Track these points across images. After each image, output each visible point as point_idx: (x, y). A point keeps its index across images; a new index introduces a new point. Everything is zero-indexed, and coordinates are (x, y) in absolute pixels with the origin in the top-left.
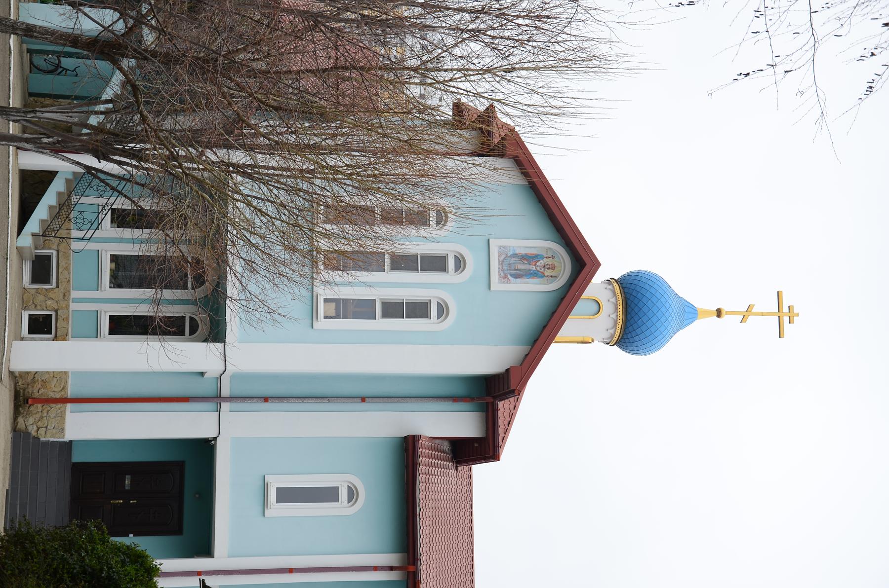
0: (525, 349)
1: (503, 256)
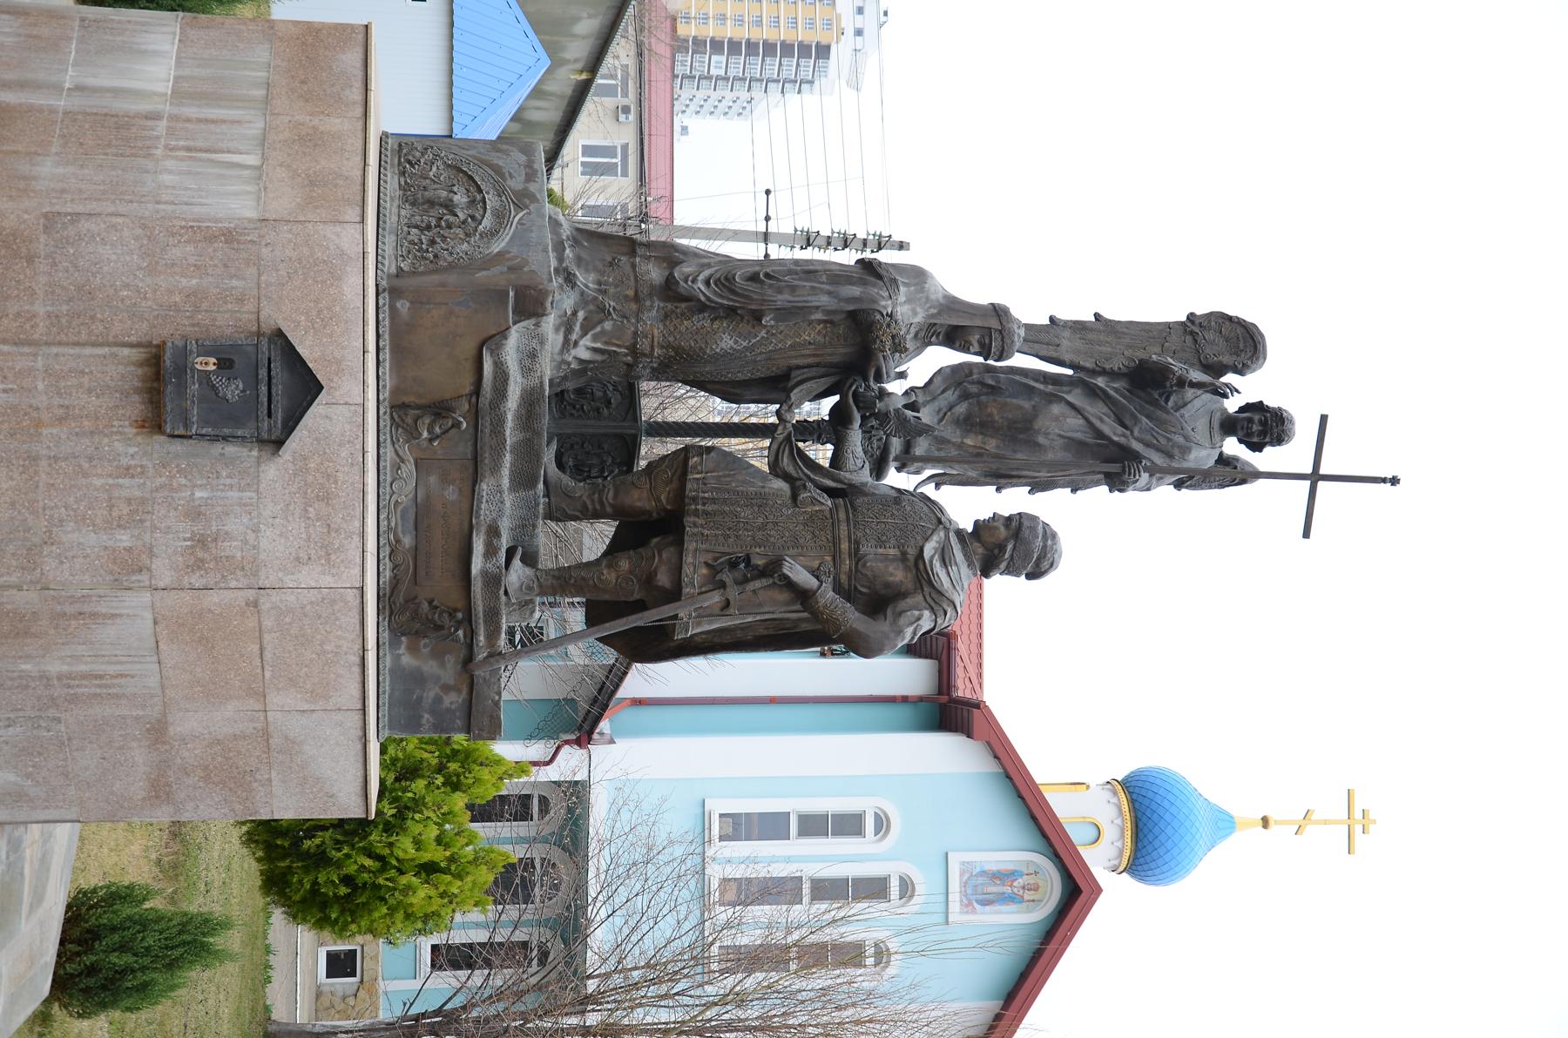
0: (995, 1005)
1: (966, 876)
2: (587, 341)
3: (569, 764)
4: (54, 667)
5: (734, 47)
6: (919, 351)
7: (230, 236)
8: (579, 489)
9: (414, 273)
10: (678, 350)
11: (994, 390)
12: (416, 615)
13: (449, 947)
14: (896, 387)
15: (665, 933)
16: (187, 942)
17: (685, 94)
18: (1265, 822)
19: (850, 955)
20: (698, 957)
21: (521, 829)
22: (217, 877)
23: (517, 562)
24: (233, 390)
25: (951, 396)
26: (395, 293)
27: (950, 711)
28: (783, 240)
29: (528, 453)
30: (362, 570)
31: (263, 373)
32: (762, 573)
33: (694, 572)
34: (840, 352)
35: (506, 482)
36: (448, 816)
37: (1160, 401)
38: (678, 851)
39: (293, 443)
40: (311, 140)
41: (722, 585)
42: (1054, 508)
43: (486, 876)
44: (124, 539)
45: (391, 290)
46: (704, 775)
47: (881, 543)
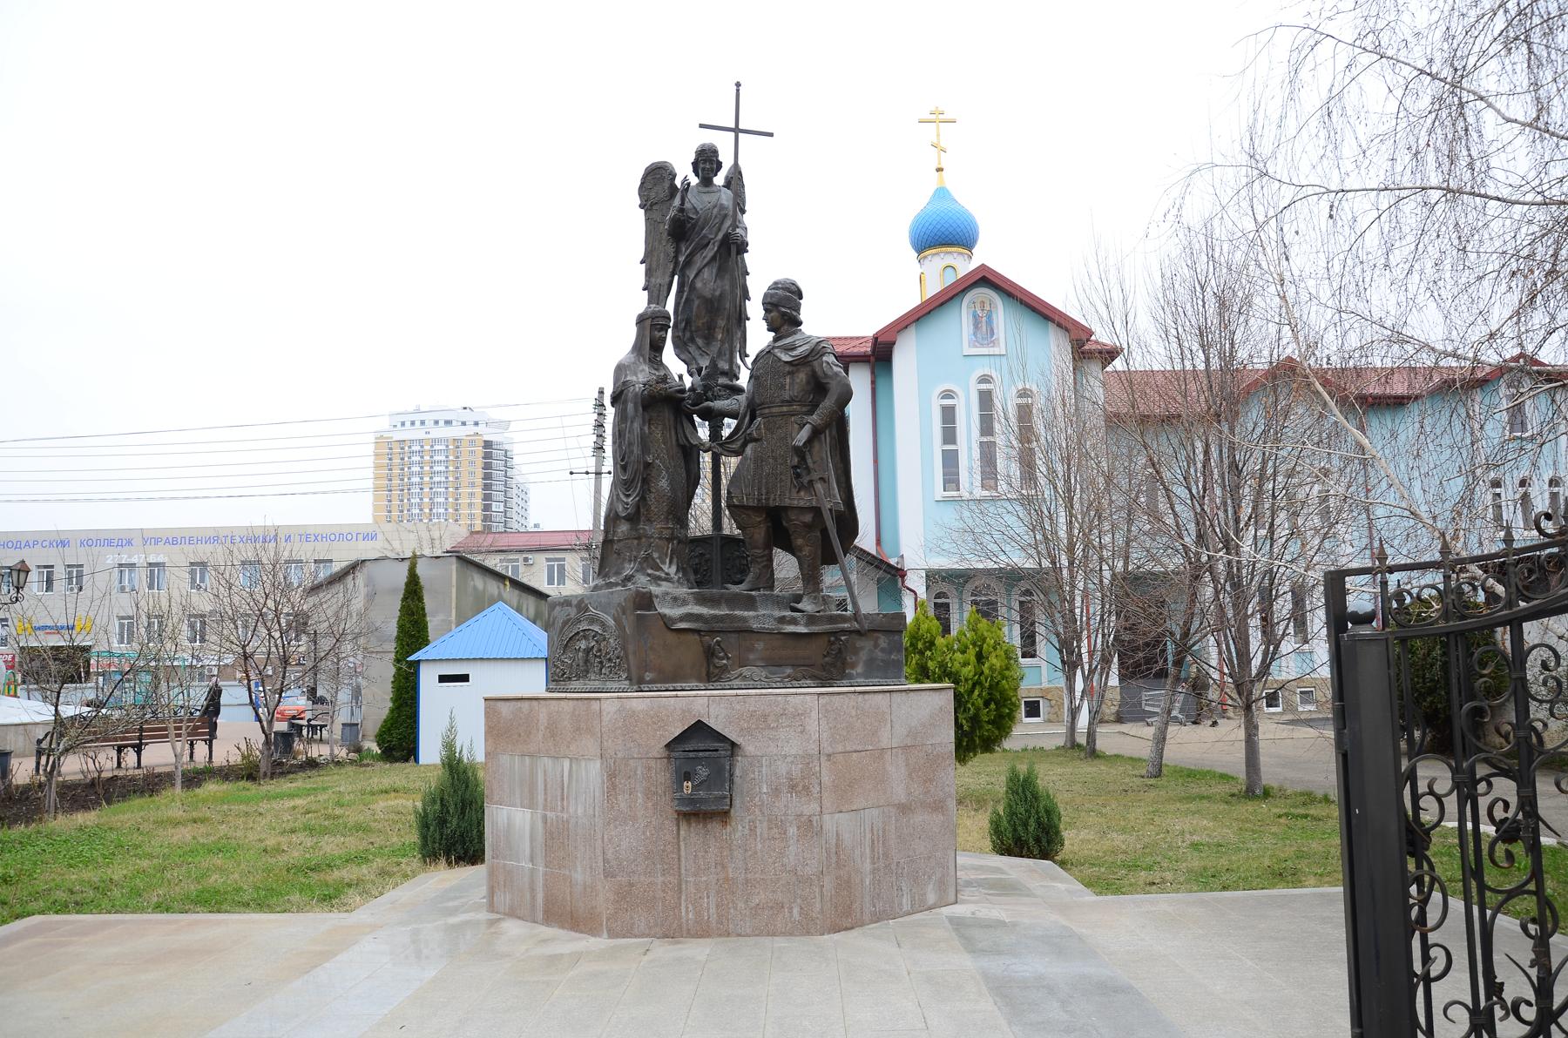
0: (1052, 328)
2: (665, 568)
3: (916, 581)
4: (868, 866)
5: (487, 497)
6: (665, 368)
7: (612, 776)
8: (754, 570)
9: (629, 670)
10: (669, 513)
11: (688, 322)
12: (833, 665)
13: (1023, 646)
14: (688, 382)
15: (1014, 521)
16: (1023, 790)
17: (516, 526)
18: (939, 170)
19: (1024, 413)
20: (1026, 501)
21: (954, 608)
22: (983, 779)
23: (799, 606)
24: (703, 772)
25: (692, 349)
26: (641, 681)
27: (879, 355)
28: (600, 461)
29: (734, 601)
30: (806, 698)
31: (691, 755)
32: (803, 458)
33: (803, 499)
34: (667, 415)
35: (751, 613)
36: (950, 648)
37: (692, 229)
38: (966, 514)
39: (733, 737)
40: (553, 731)
41: (811, 482)
42: (758, 286)
43: (984, 624)
44: (792, 831)
45: (639, 683)
46: (922, 501)
47: (783, 386)
